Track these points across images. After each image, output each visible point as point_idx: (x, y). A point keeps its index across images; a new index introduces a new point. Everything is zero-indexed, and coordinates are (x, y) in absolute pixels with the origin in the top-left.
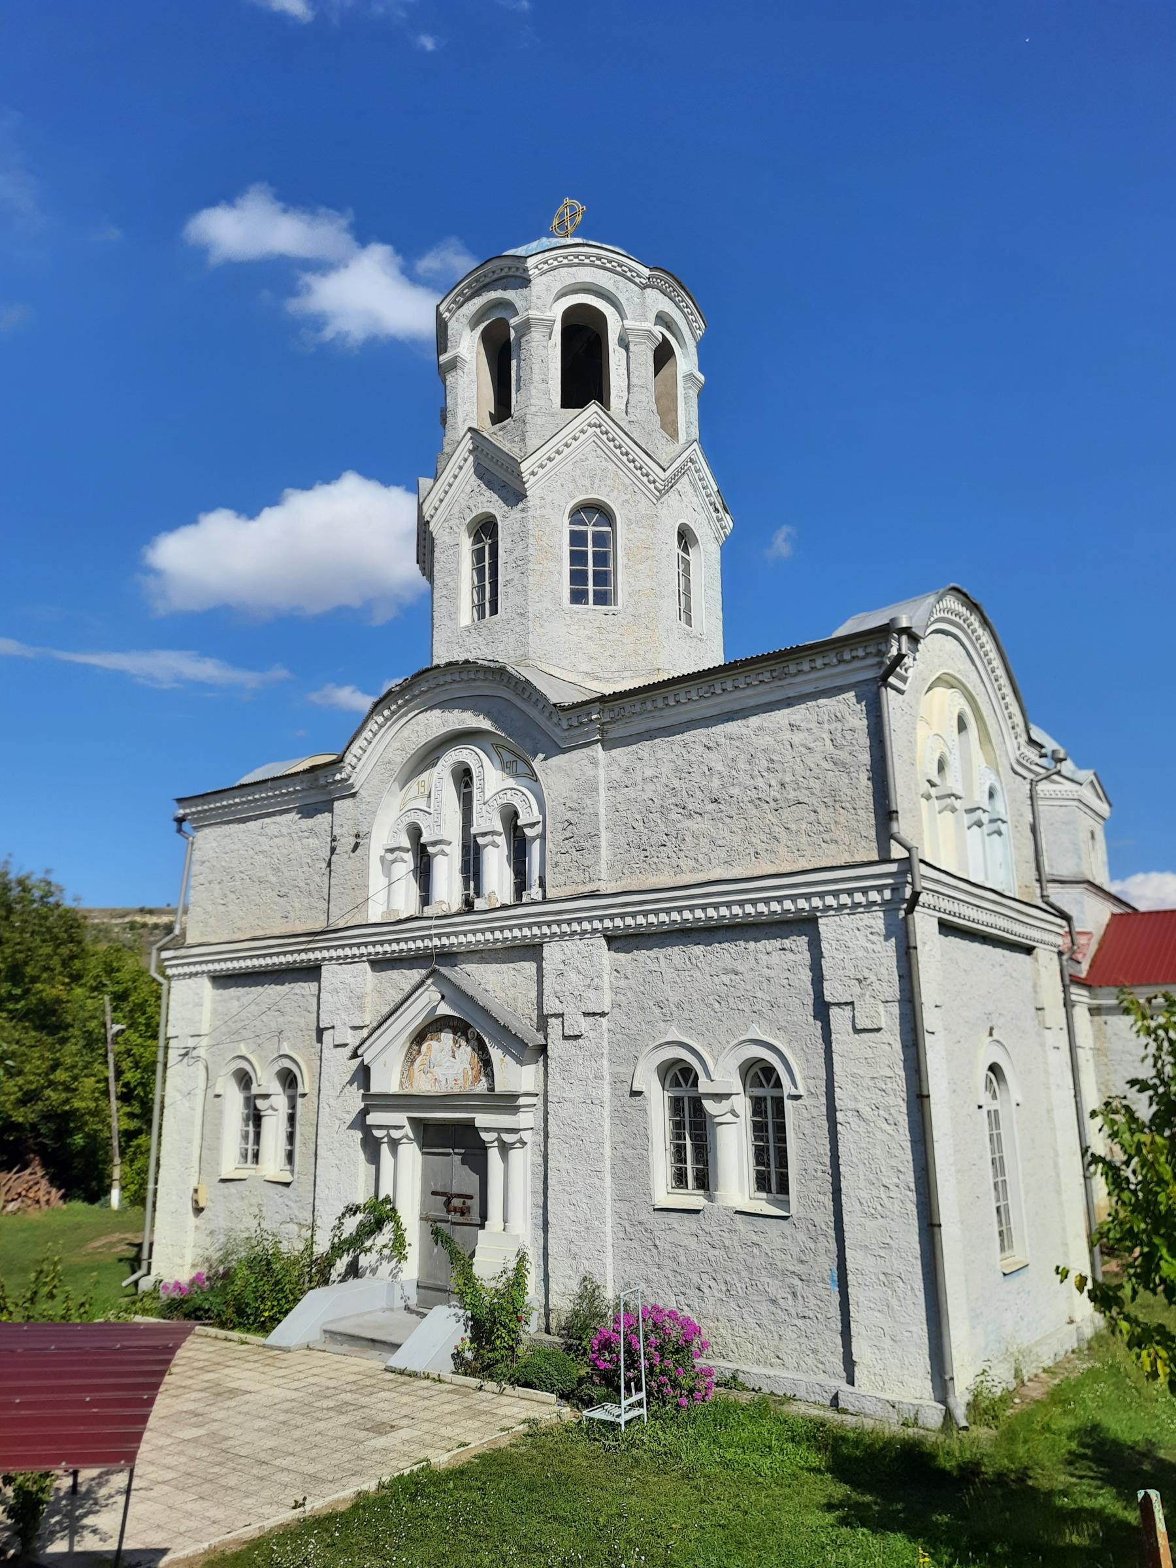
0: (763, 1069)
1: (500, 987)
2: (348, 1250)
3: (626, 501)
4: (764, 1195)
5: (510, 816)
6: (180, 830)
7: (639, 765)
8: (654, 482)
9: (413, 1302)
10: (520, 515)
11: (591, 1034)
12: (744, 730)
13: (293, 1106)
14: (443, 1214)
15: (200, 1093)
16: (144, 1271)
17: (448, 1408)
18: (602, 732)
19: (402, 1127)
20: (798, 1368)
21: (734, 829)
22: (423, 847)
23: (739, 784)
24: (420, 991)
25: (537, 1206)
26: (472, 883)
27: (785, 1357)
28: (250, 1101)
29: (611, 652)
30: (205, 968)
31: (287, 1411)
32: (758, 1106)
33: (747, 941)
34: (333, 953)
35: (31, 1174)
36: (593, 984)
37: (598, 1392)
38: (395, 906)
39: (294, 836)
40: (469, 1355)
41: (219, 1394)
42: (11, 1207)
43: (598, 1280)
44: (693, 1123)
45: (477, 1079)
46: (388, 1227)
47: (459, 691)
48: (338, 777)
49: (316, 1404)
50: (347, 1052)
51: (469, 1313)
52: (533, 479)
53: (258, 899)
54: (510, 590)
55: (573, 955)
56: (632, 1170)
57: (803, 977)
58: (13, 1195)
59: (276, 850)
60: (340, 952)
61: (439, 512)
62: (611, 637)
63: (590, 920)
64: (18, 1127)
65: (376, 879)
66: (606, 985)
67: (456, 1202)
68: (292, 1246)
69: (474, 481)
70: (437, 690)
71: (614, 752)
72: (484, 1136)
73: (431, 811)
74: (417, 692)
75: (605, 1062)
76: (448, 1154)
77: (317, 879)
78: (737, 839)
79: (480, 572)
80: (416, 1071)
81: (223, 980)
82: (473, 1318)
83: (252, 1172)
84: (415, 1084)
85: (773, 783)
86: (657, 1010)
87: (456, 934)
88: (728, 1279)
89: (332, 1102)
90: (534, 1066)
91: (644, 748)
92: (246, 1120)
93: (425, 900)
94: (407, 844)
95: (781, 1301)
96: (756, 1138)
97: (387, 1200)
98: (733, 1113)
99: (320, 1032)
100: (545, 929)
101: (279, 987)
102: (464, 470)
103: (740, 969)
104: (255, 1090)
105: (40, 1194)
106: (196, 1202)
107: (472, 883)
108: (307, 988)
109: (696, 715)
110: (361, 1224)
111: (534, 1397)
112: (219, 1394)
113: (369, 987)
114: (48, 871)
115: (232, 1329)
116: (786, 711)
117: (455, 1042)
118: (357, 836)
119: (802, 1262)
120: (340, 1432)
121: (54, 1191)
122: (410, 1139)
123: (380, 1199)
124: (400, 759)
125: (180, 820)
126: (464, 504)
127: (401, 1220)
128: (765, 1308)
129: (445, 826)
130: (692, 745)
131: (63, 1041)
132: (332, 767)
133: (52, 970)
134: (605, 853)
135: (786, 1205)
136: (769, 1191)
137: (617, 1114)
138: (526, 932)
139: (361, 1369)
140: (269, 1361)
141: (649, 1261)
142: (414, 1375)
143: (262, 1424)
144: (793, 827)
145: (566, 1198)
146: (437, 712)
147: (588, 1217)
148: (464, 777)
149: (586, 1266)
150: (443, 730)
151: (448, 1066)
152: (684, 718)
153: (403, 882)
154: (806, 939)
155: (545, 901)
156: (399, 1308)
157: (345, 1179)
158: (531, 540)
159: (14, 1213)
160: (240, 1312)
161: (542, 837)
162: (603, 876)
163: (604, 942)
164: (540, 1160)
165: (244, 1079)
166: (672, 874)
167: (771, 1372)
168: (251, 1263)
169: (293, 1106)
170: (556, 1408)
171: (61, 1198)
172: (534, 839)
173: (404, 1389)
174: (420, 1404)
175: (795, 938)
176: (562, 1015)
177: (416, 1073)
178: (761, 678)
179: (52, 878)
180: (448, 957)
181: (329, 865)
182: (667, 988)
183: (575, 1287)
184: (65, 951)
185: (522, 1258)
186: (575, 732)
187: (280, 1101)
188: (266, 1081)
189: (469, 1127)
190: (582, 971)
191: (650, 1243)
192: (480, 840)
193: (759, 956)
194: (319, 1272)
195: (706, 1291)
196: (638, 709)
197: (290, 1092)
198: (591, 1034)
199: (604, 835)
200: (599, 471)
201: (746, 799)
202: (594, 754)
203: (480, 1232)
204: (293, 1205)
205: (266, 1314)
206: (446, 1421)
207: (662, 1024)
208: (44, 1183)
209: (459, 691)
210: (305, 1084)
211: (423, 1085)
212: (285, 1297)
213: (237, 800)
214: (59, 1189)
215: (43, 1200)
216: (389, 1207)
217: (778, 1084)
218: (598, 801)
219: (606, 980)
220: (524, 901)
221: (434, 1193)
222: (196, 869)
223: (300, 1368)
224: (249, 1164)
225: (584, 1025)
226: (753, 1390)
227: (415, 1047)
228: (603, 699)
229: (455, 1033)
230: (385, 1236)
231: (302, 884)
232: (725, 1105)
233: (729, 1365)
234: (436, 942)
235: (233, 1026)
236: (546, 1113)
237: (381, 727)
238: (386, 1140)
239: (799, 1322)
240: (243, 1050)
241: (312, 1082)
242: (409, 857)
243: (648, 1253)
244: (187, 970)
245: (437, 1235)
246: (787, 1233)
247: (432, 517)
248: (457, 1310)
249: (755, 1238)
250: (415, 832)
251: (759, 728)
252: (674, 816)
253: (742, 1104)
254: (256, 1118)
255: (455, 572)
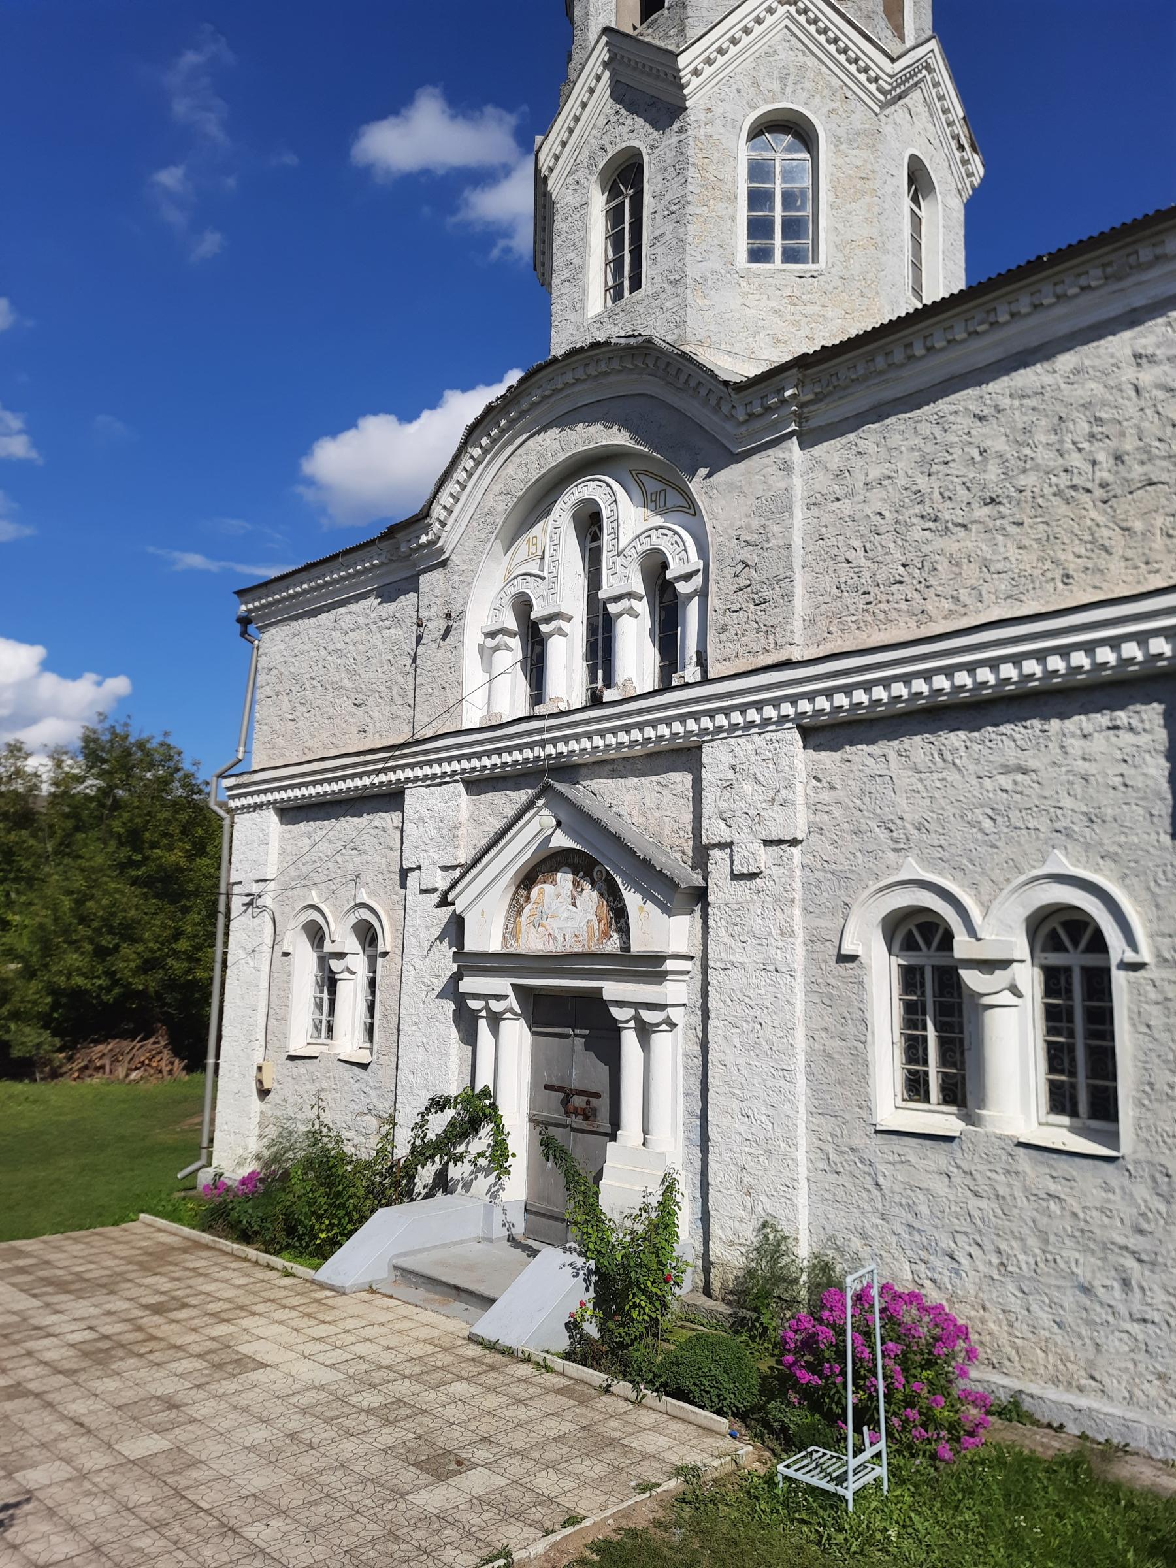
0: (1066, 925)
1: (644, 809)
2: (432, 1157)
3: (833, 111)
4: (1065, 1120)
5: (655, 570)
6: (244, 633)
7: (858, 463)
8: (876, 79)
9: (519, 1230)
10: (675, 139)
11: (775, 871)
12: (1048, 379)
13: (373, 970)
14: (559, 1116)
15: (266, 950)
16: (203, 1161)
17: (554, 1427)
18: (800, 418)
19: (504, 997)
20: (1130, 1399)
21: (1026, 542)
22: (534, 625)
23: (1037, 468)
24: (528, 815)
25: (691, 1113)
26: (600, 672)
27: (1106, 1380)
28: (323, 961)
29: (808, 332)
30: (270, 797)
31: (305, 1411)
32: (1054, 981)
33: (1046, 718)
34: (419, 772)
35: (155, 1043)
36: (780, 798)
37: (796, 1417)
38: (496, 709)
39: (373, 627)
40: (591, 1329)
41: (219, 1366)
42: (134, 1075)
43: (786, 1228)
44: (941, 1006)
45: (606, 935)
46: (486, 1130)
47: (586, 395)
48: (424, 539)
49: (355, 1400)
50: (435, 898)
51: (592, 1264)
52: (695, 82)
53: (331, 711)
54: (660, 250)
55: (747, 756)
56: (841, 1069)
57: (1152, 771)
58: (136, 1063)
59: (351, 648)
60: (427, 771)
61: (561, 161)
62: (809, 309)
63: (775, 703)
64: (142, 995)
65: (473, 673)
66: (800, 800)
67: (578, 1101)
68: (361, 1145)
69: (610, 106)
70: (553, 399)
71: (819, 450)
72: (616, 1012)
73: (545, 574)
74: (525, 406)
75: (797, 912)
76: (567, 1036)
77: (401, 680)
78: (1030, 558)
79: (616, 241)
80: (524, 924)
81: (291, 813)
82: (597, 1271)
83: (324, 1049)
84: (522, 941)
85: (1101, 457)
86: (882, 834)
87: (577, 737)
88: (1003, 1246)
89: (419, 964)
90: (688, 917)
91: (869, 437)
92: (320, 986)
93: (538, 697)
94: (512, 624)
95: (1100, 1291)
96: (1050, 1031)
97: (486, 1092)
98: (1014, 990)
99: (404, 873)
100: (706, 722)
101: (355, 820)
102: (596, 95)
103: (1032, 764)
104: (328, 947)
105: (163, 1063)
106: (260, 1082)
107: (600, 672)
108: (390, 819)
109: (958, 368)
110: (452, 1124)
111: (692, 1418)
112: (219, 1366)
113: (464, 815)
114: (166, 734)
115: (277, 1253)
116: (1127, 335)
117: (576, 884)
118: (448, 616)
119: (1141, 1232)
120: (375, 1467)
121: (177, 1061)
122: (514, 1013)
123: (477, 1091)
124: (502, 506)
125: (245, 621)
126: (595, 143)
127: (504, 1121)
128: (1070, 1298)
129: (568, 595)
130: (951, 418)
131: (186, 910)
132: (416, 526)
133: (172, 836)
134: (800, 604)
135: (1112, 1139)
136: (1074, 1114)
137: (815, 988)
138: (677, 727)
139: (436, 1333)
140: (311, 1309)
141: (867, 1207)
142: (508, 1352)
143: (259, 1434)
144: (1138, 525)
145: (736, 1105)
146: (553, 433)
147: (770, 1134)
148: (590, 524)
149: (767, 1206)
150: (562, 457)
151: (566, 916)
152: (938, 376)
153: (507, 677)
154: (1158, 707)
155: (705, 681)
156: (500, 1239)
157: (435, 1064)
158: (691, 172)
159: (137, 1082)
160: (291, 1231)
161: (703, 593)
162: (797, 639)
163: (797, 736)
164: (697, 1050)
165: (316, 934)
166: (913, 624)
167: (1083, 1402)
168: (309, 1163)
169: (373, 970)
170: (728, 1444)
171: (183, 1069)
172: (690, 597)
173: (491, 1379)
174: (510, 1413)
175: (1139, 707)
176: (730, 845)
177: (524, 927)
178: (1083, 281)
179: (169, 741)
180: (568, 770)
181: (414, 661)
182: (901, 800)
183: (750, 1235)
184: (184, 817)
185: (670, 1186)
186: (757, 424)
187: (358, 962)
188: (341, 937)
189: (594, 1003)
190: (766, 782)
191: (868, 1180)
192: (612, 608)
193: (1068, 741)
194: (393, 1184)
195: (965, 1261)
196: (861, 370)
197: (369, 950)
198: (775, 871)
199: (799, 577)
200: (793, 69)
201: (1048, 491)
202: (786, 456)
203: (610, 1145)
204: (373, 1093)
205: (323, 1236)
206: (549, 1456)
207: (891, 855)
208: (166, 1055)
209: (586, 395)
210: (386, 942)
211: (533, 943)
212: (349, 1214)
213: (305, 586)
214: (182, 1059)
215: (166, 1069)
216: (488, 1102)
217: (1099, 943)
218: (791, 526)
219: (800, 791)
220: (673, 684)
221: (548, 1087)
222: (262, 678)
223: (350, 1324)
224: (323, 1040)
225: (763, 858)
226: (1049, 1426)
227: (523, 892)
228: (802, 362)
229: (575, 873)
230: (481, 1142)
231: (382, 688)
232: (1000, 978)
233: (1005, 1381)
234: (550, 750)
235: (304, 869)
236: (705, 983)
237: (478, 462)
238: (484, 1013)
239: (1135, 1328)
240: (315, 899)
241: (394, 938)
242: (515, 643)
243: (864, 1194)
244: (250, 800)
245: (549, 1147)
246: (1114, 1183)
247: (551, 170)
248: (574, 1257)
249: (1053, 1187)
250: (523, 605)
251: (1077, 371)
252: (917, 534)
253: (1028, 977)
254: (330, 982)
255: (580, 245)
